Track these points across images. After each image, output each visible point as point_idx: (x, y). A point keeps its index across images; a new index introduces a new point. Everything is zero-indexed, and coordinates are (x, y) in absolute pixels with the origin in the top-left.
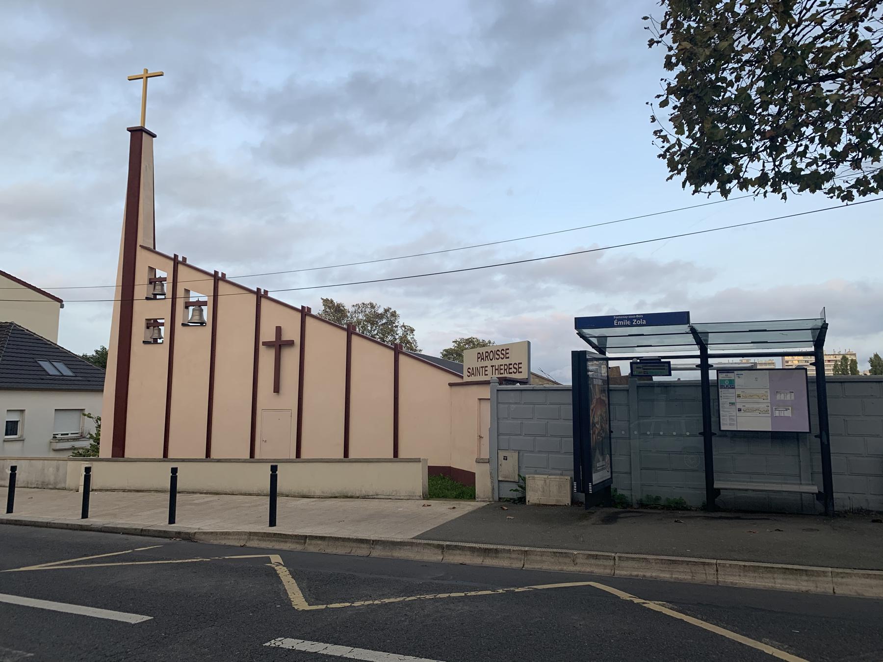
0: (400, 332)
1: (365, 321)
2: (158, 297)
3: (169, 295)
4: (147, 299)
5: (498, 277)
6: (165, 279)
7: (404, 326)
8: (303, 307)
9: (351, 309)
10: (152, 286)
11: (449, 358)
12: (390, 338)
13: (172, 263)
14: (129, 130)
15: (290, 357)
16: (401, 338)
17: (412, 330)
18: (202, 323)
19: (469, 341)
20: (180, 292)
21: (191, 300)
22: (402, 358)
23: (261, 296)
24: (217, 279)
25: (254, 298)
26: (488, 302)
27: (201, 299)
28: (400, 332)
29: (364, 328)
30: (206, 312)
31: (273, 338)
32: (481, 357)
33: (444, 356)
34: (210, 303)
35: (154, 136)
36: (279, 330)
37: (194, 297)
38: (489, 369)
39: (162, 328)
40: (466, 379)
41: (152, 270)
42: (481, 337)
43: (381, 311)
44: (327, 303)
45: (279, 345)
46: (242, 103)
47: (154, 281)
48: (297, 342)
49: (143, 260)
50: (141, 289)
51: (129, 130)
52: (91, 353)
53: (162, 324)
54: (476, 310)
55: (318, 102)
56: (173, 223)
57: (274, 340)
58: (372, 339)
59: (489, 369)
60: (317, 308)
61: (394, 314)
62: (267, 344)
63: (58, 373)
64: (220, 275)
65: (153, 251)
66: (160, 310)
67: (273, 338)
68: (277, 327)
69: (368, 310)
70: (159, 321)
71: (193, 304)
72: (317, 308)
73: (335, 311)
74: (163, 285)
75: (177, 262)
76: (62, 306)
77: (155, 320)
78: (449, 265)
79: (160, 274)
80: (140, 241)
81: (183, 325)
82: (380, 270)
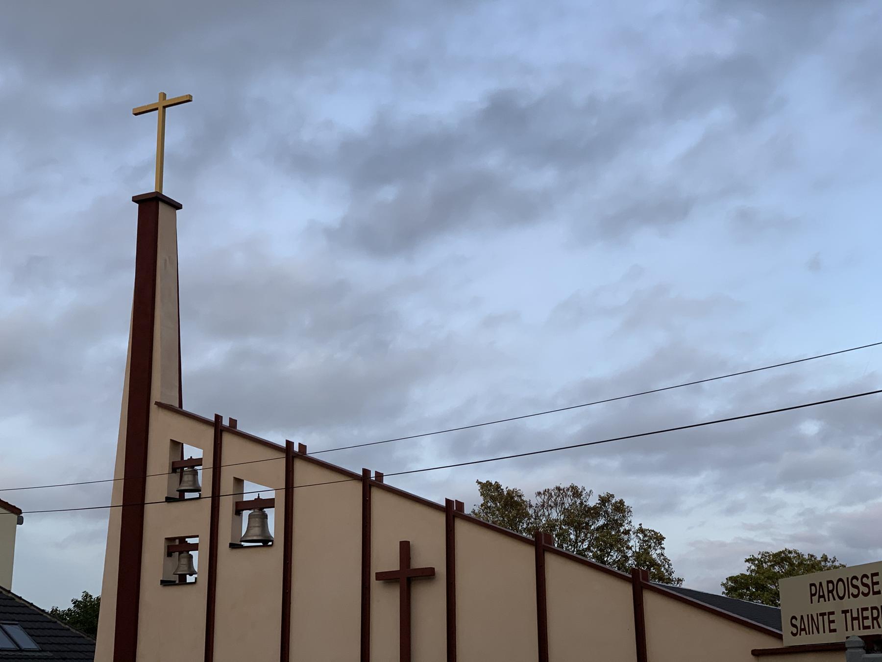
0: (635, 543)
1: (565, 522)
2: (188, 495)
3: (207, 491)
4: (169, 500)
5: (810, 427)
6: (199, 462)
7: (641, 530)
8: (447, 501)
9: (536, 501)
10: (176, 477)
11: (741, 595)
12: (615, 555)
13: (211, 432)
14: (136, 199)
15: (430, 602)
16: (637, 556)
17: (659, 539)
18: (266, 542)
19: (781, 558)
20: (227, 485)
21: (247, 498)
22: (552, 563)
23: (370, 483)
24: (292, 455)
25: (357, 488)
26: (797, 477)
27: (263, 496)
28: (635, 543)
29: (563, 536)
30: (273, 519)
31: (396, 567)
32: (817, 593)
33: (730, 590)
34: (281, 503)
35: (178, 206)
36: (405, 548)
37: (252, 491)
38: (838, 617)
39: (195, 554)
40: (789, 641)
41: (177, 446)
42: (805, 549)
43: (593, 502)
44: (489, 489)
45: (408, 578)
46: (304, 164)
47: (181, 467)
48: (441, 569)
49: (162, 428)
50: (158, 484)
51: (136, 199)
52: (65, 605)
53: (195, 547)
54: (778, 494)
55: (429, 149)
56: (205, 362)
57: (398, 568)
58: (579, 560)
59: (838, 617)
60: (473, 501)
61: (620, 507)
62: (386, 577)
63: (11, 646)
64: (296, 448)
65: (178, 410)
66: (190, 519)
67: (396, 567)
68: (401, 543)
69: (568, 502)
70: (189, 541)
71: (249, 505)
72: (473, 501)
73: (505, 506)
74: (195, 473)
75: (221, 429)
76: (20, 521)
77: (182, 540)
78: (708, 407)
79: (191, 452)
80: (157, 394)
81: (233, 546)
82: (568, 426)
